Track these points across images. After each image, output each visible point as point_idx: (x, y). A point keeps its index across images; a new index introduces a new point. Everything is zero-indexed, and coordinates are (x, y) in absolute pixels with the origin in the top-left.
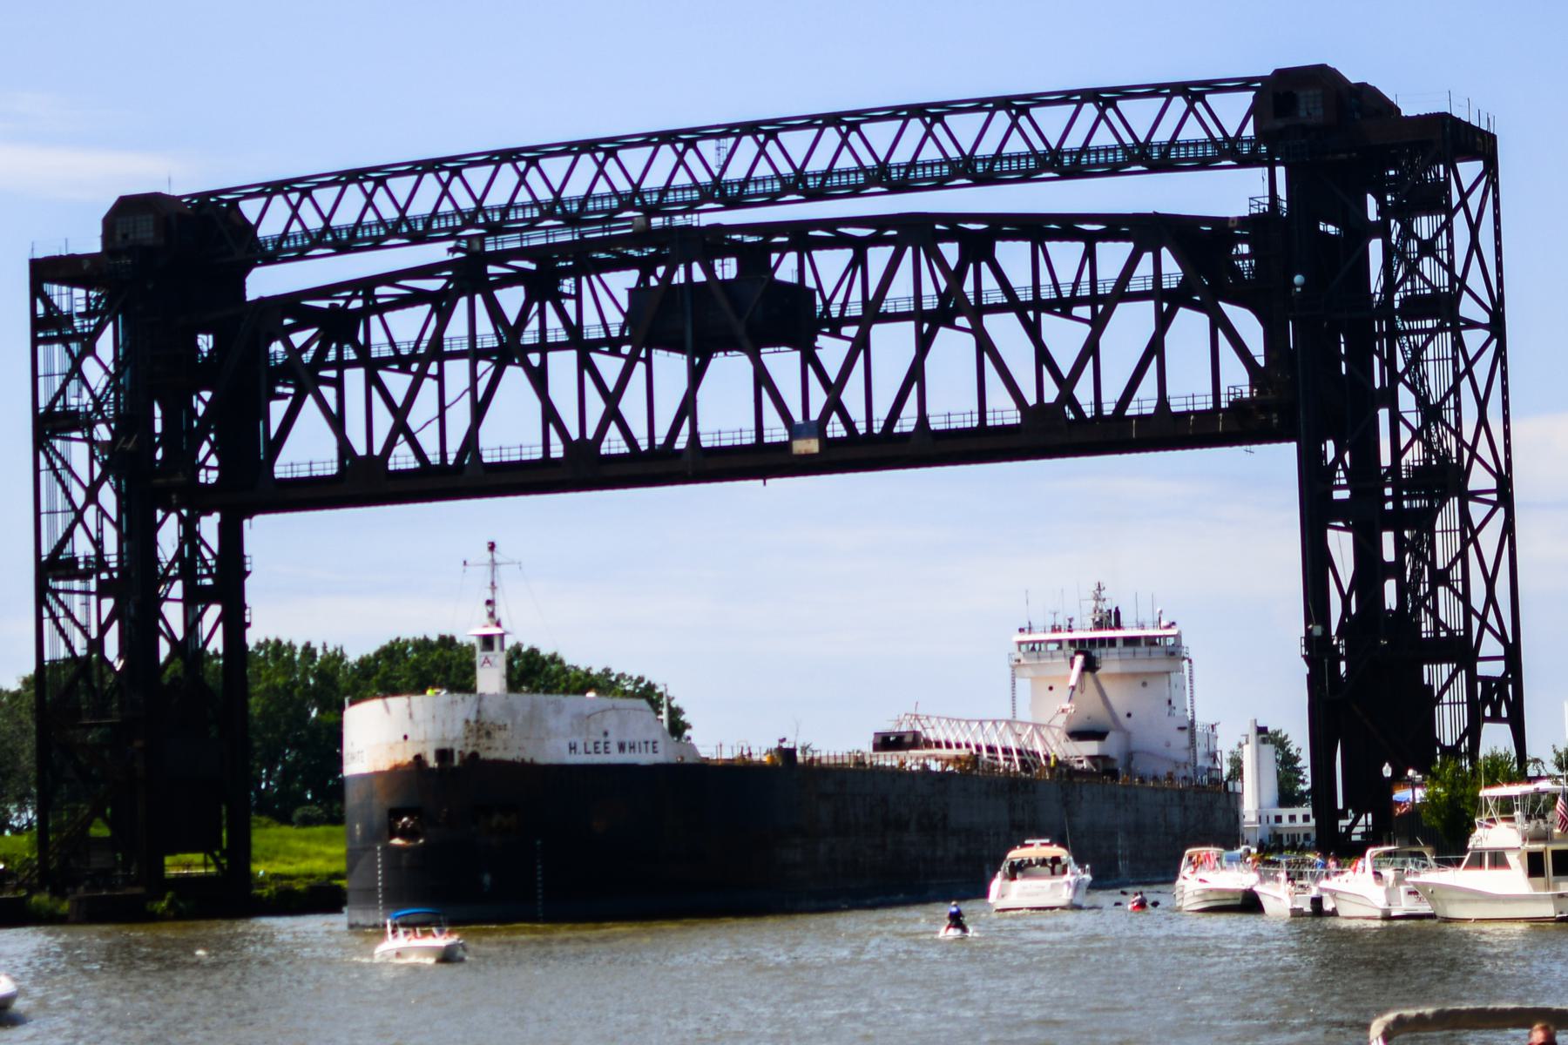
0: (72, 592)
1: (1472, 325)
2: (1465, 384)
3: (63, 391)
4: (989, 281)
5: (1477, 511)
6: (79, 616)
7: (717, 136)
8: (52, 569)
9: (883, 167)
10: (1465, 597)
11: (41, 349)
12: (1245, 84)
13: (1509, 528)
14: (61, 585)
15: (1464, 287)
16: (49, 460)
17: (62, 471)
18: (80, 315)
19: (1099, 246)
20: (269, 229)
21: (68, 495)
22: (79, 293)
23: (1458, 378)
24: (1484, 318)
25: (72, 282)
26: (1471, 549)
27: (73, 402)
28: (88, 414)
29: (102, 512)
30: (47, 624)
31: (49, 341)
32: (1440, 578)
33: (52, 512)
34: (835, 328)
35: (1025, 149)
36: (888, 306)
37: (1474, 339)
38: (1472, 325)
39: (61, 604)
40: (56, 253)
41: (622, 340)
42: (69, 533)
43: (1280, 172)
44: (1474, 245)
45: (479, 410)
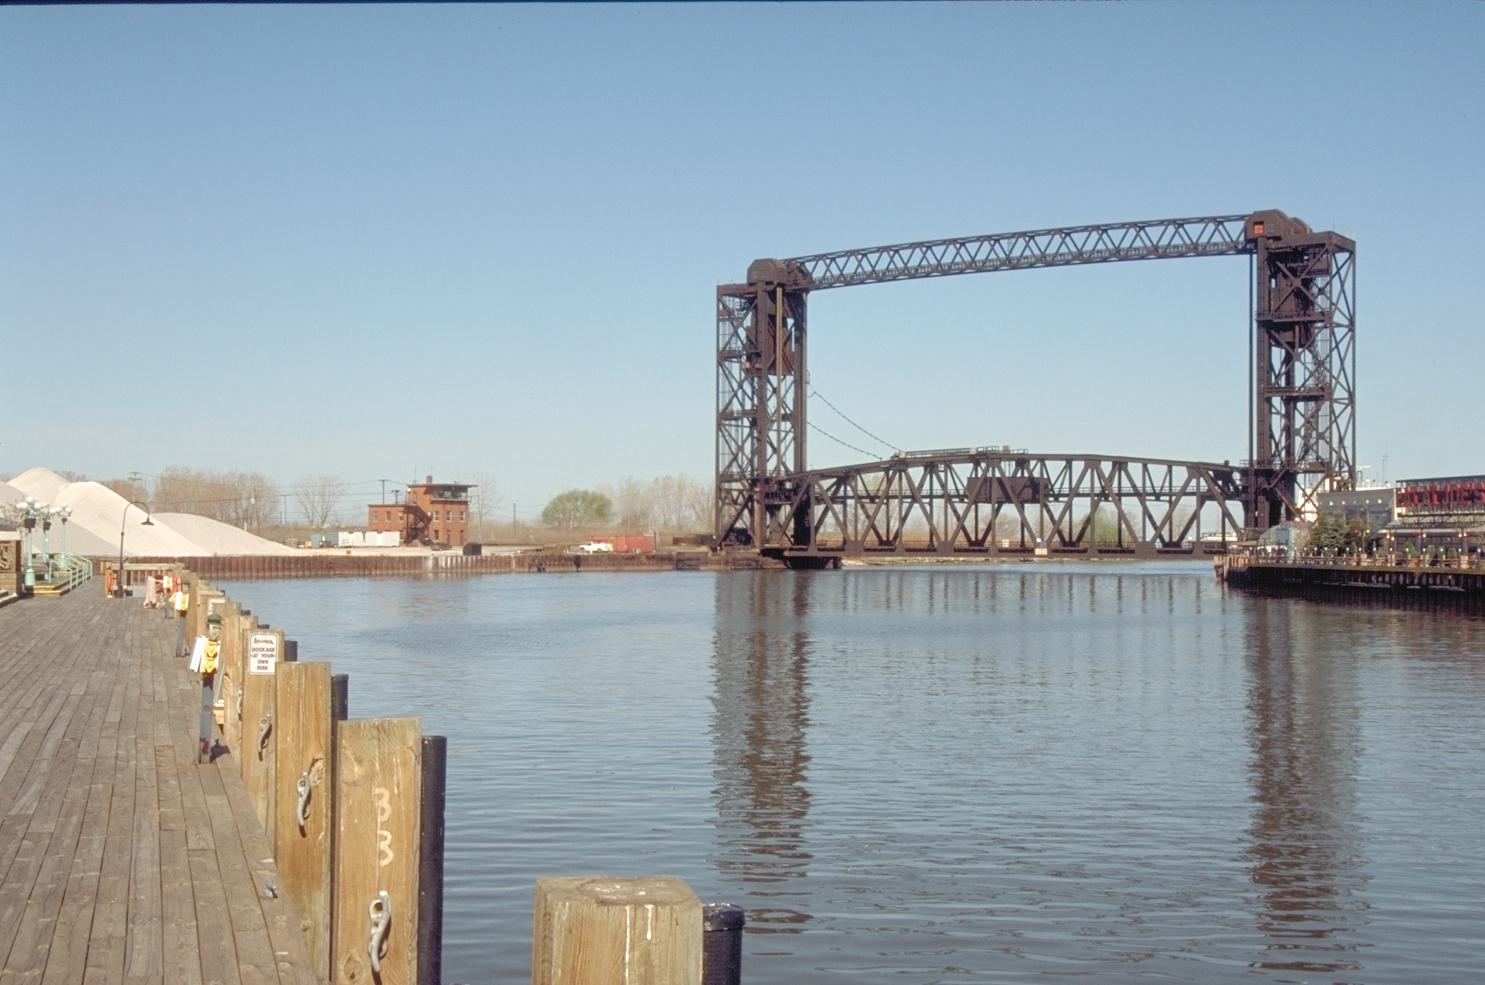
0: (731, 425)
1: (1339, 325)
2: (1335, 353)
3: (729, 342)
4: (1125, 483)
5: (1338, 408)
6: (733, 435)
7: (1008, 238)
8: (724, 416)
9: (1080, 253)
10: (1330, 443)
11: (721, 324)
12: (1242, 218)
13: (1353, 415)
14: (727, 422)
15: (1337, 308)
16: (724, 371)
17: (728, 376)
18: (738, 310)
19: (1174, 468)
20: (818, 274)
21: (730, 448)
22: (737, 300)
23: (1331, 350)
24: (1346, 322)
25: (733, 295)
26: (1334, 425)
27: (734, 346)
28: (739, 352)
29: (744, 393)
30: (721, 439)
31: (723, 320)
32: (1320, 436)
33: (723, 454)
34: (1057, 497)
35: (1142, 245)
36: (1081, 491)
37: (1340, 332)
38: (1339, 325)
39: (727, 431)
40: (728, 283)
41: (965, 496)
42: (730, 402)
43: (1255, 256)
44: (1343, 291)
45: (903, 520)
